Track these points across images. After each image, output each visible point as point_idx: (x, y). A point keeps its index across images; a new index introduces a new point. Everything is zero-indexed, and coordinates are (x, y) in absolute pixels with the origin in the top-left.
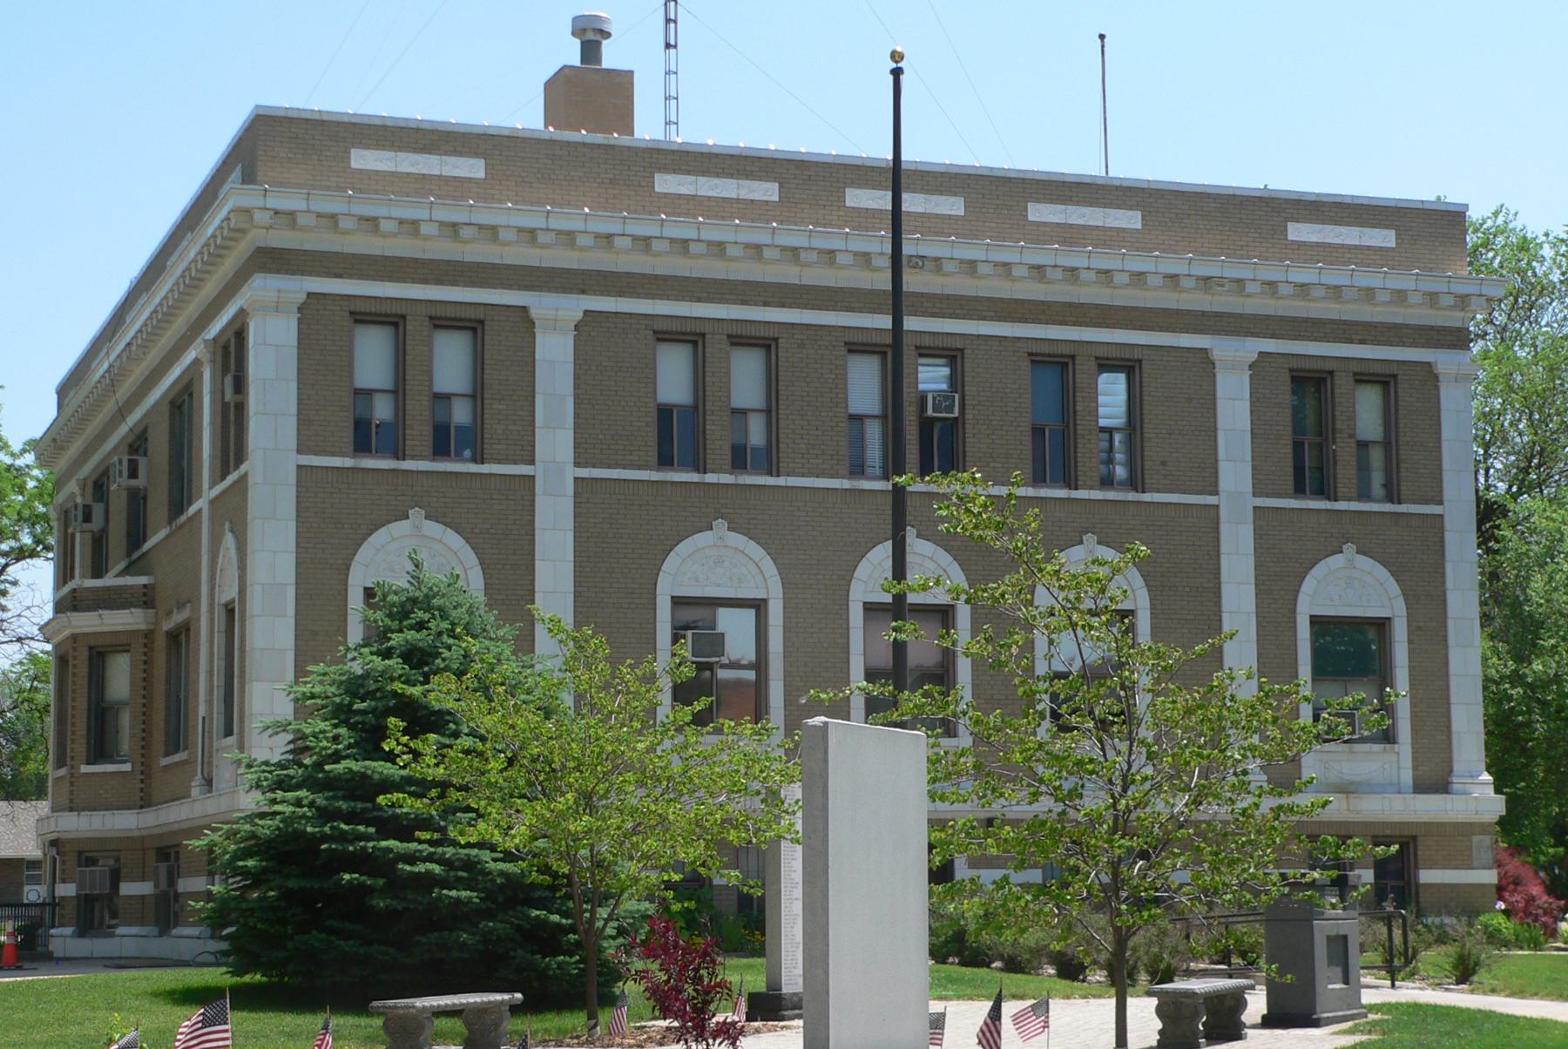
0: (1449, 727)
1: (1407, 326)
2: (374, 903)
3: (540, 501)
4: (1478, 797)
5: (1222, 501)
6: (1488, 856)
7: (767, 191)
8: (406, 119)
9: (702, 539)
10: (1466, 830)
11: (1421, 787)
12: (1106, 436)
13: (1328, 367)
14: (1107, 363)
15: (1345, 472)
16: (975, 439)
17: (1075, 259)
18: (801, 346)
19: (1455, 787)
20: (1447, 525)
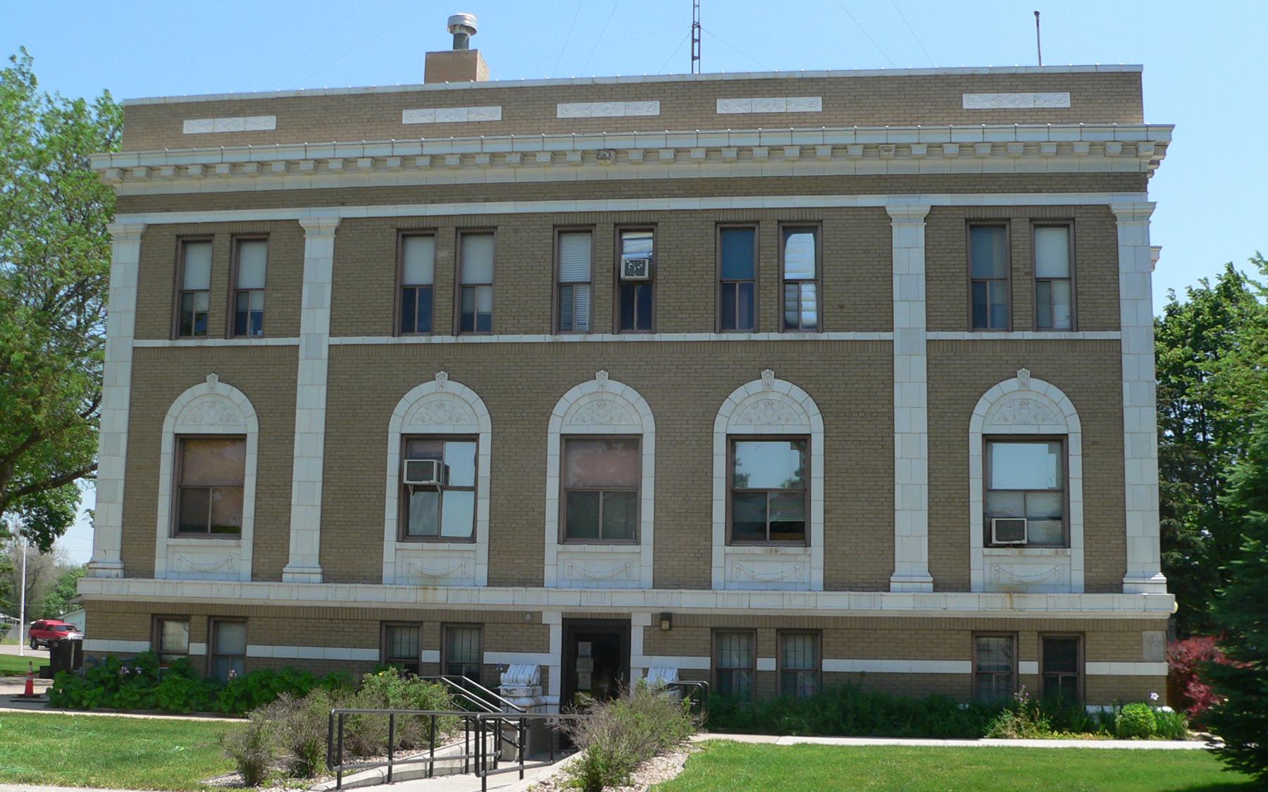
1: (1083, 174)
3: (302, 364)
4: (1151, 595)
5: (896, 336)
7: (650, 108)
8: (366, 88)
10: (1135, 627)
11: (1092, 587)
13: (1007, 214)
15: (1023, 306)
16: (663, 298)
17: (749, 139)
18: (516, 231)
20: (1124, 350)
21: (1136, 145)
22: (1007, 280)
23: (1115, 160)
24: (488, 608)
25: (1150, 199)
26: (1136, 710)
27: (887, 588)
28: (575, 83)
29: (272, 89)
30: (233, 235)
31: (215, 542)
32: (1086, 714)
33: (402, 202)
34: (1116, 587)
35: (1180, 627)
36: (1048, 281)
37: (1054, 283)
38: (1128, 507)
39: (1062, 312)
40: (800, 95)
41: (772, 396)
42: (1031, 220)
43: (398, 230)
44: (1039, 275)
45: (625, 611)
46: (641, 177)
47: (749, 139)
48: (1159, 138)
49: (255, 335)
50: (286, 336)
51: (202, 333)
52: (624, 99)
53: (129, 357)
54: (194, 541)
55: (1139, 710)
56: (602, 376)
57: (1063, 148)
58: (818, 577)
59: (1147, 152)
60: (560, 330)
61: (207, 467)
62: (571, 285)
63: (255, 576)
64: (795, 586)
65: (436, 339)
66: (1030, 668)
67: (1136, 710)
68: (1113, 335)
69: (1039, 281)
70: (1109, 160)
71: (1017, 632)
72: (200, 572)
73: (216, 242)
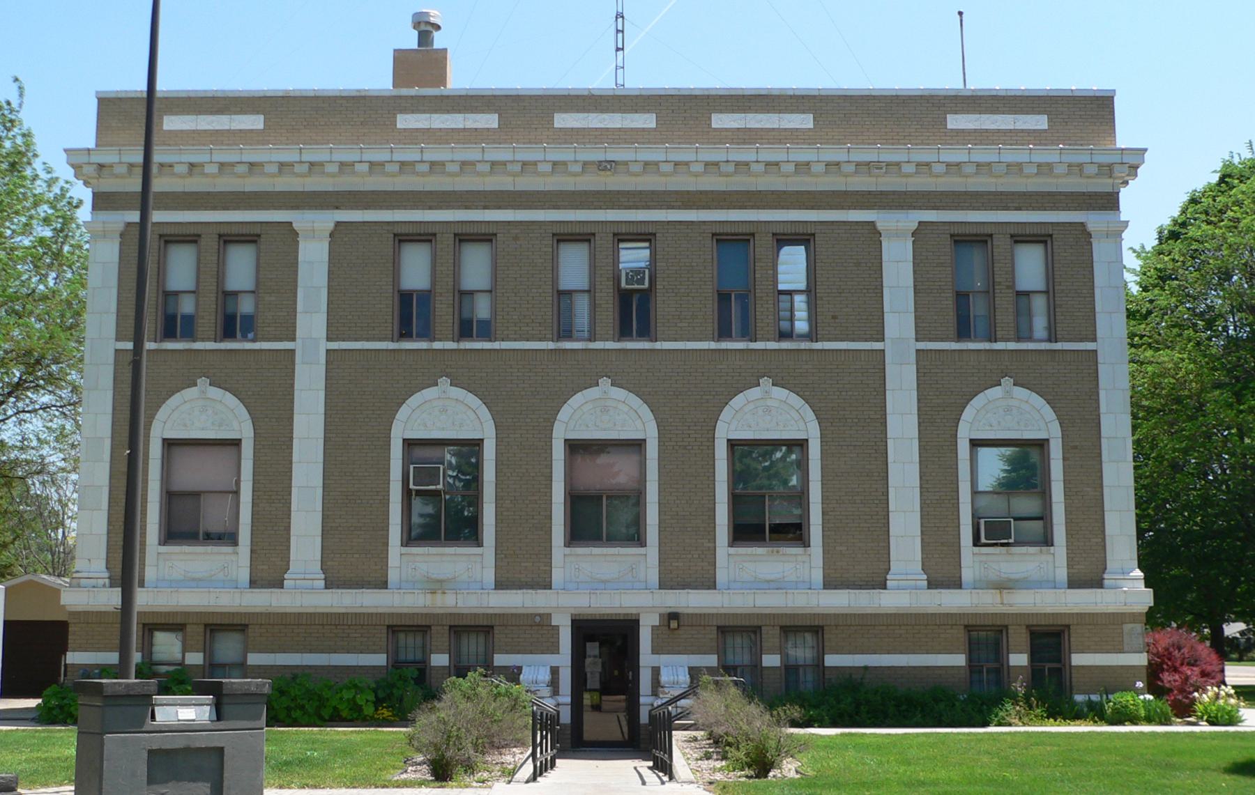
0: (1103, 531)
2: (810, 686)
4: (1130, 590)
5: (887, 346)
6: (1140, 642)
8: (358, 91)
9: (429, 393)
10: (1117, 620)
11: (1075, 583)
12: (788, 297)
13: (988, 230)
14: (785, 237)
15: (1005, 317)
16: (663, 307)
18: (516, 238)
19: (1106, 582)
20: (1100, 360)
21: (1110, 166)
22: (990, 292)
23: (1090, 180)
24: (497, 611)
25: (1123, 218)
26: (1127, 698)
27: (883, 586)
28: (572, 93)
29: (226, 88)
30: (220, 236)
31: (209, 549)
32: (1075, 703)
33: (399, 208)
34: (1096, 582)
35: (1153, 619)
36: (569, 293)
37: (577, 297)
38: (891, 508)
39: (1040, 324)
40: (792, 112)
41: (769, 403)
42: (1012, 236)
43: (395, 235)
44: (562, 287)
45: (634, 611)
46: (639, 189)
47: (984, 155)
48: (1133, 161)
49: (245, 338)
50: (281, 340)
51: (189, 334)
52: (620, 110)
53: (323, 360)
54: (216, 549)
55: (1129, 698)
56: (605, 382)
57: (1045, 169)
58: (818, 576)
59: (1119, 172)
60: (560, 337)
61: (196, 473)
62: (471, 293)
63: (253, 583)
64: (796, 585)
65: (437, 345)
66: (1019, 659)
67: (1127, 698)
68: (1089, 346)
70: (1084, 181)
71: (1006, 627)
72: (194, 580)
73: (203, 242)
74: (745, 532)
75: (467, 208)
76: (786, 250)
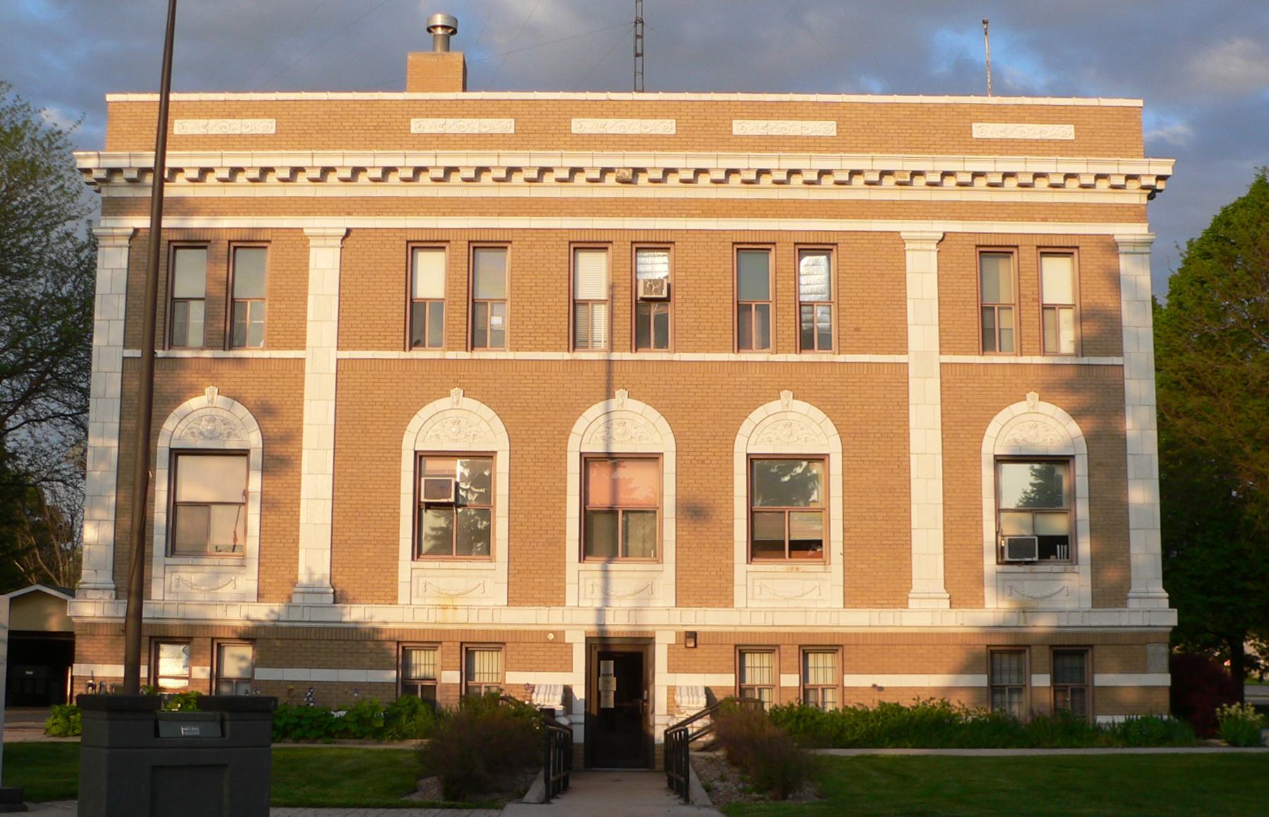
9: (1019, 408)
18: (531, 246)
45: (649, 629)
69: (1045, 308)
74: (762, 548)
75: (481, 214)
76: (807, 260)
